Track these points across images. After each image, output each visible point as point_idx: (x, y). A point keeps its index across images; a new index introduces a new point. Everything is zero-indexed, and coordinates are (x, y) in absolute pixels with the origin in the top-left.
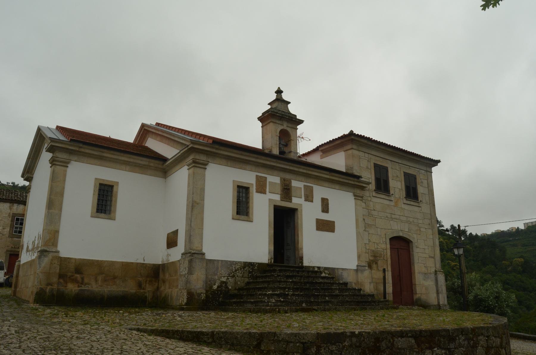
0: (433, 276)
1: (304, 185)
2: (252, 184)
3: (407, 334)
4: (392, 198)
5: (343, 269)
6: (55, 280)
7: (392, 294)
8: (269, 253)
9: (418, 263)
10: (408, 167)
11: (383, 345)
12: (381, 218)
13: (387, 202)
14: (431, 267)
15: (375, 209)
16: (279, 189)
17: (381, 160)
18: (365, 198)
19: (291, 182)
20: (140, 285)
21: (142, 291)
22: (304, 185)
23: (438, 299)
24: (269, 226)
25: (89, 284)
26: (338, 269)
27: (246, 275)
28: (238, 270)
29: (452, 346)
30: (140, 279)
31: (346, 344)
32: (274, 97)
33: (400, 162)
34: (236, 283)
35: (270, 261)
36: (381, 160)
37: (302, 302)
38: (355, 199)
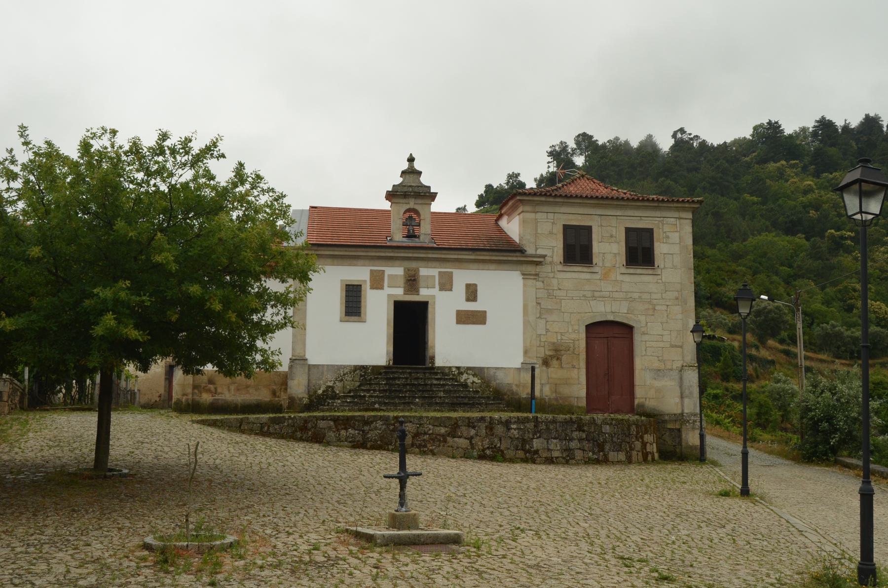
0: (675, 374)
1: (439, 272)
2: (365, 281)
3: (327, 418)
4: (596, 269)
5: (497, 368)
6: (189, 390)
7: (585, 399)
8: (387, 354)
9: (645, 355)
10: (639, 218)
11: (309, 425)
12: (573, 299)
13: (588, 276)
14: (673, 361)
15: (560, 288)
16: (401, 282)
17: (580, 218)
18: (542, 274)
19: (419, 270)
20: (274, 393)
21: (277, 399)
22: (439, 272)
23: (683, 406)
24: (388, 324)
25: (222, 393)
26: (488, 368)
27: (357, 379)
28: (347, 373)
29: (366, 428)
30: (274, 387)
31: (286, 424)
32: (405, 166)
33: (618, 214)
34: (344, 387)
35: (388, 363)
36: (579, 217)
37: (375, 403)
38: (523, 278)
